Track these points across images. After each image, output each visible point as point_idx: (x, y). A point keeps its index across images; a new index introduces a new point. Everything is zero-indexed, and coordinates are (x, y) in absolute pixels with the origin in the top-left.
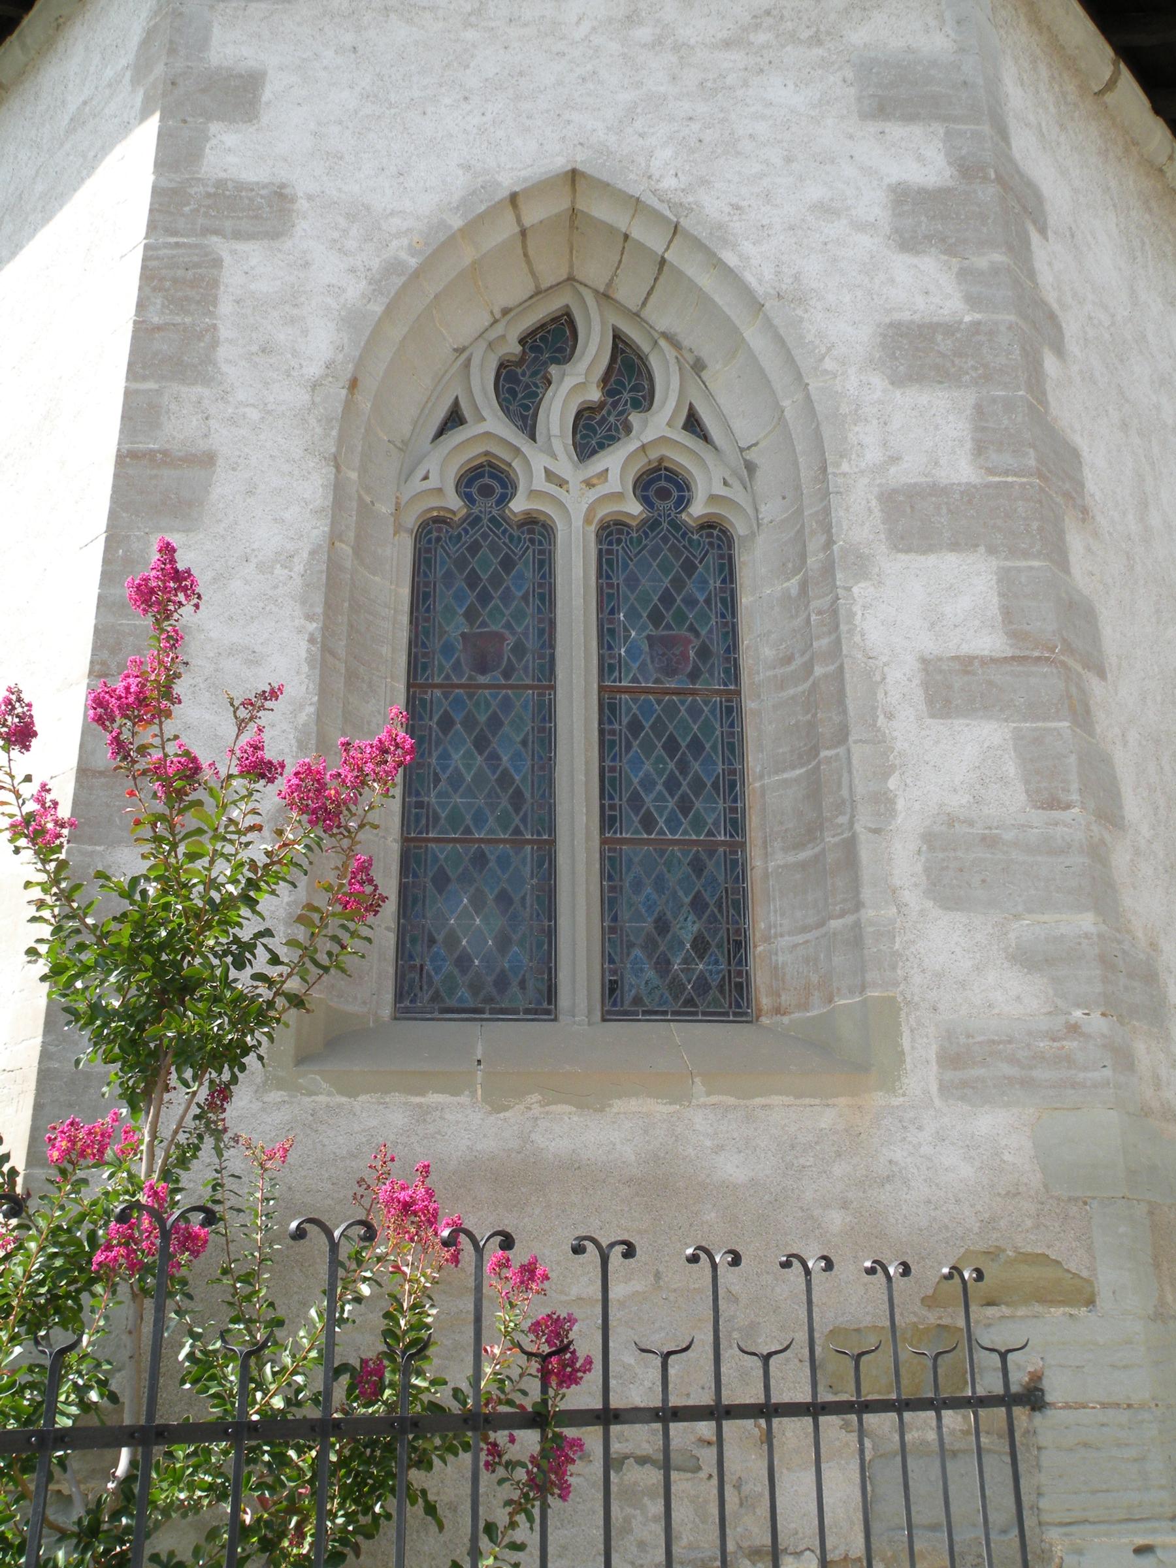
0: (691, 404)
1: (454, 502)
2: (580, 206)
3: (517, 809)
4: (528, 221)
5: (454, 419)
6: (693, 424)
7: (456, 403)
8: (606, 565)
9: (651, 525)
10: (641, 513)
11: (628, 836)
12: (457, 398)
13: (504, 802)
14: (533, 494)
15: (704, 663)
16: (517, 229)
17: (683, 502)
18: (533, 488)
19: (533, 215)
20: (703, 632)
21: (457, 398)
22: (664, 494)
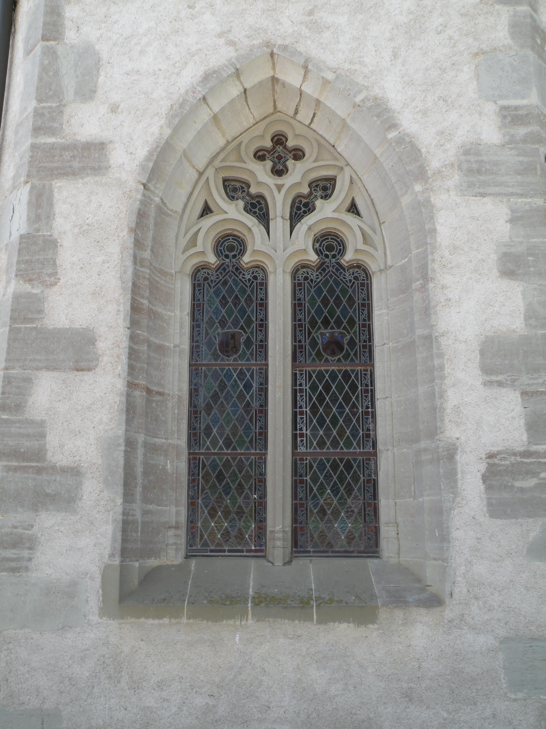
0: (353, 199)
1: (212, 259)
2: (279, 76)
3: (247, 412)
4: (248, 86)
5: (206, 210)
6: (353, 209)
7: (206, 203)
8: (297, 287)
9: (221, 268)
10: (216, 261)
11: (203, 451)
12: (206, 200)
13: (241, 410)
14: (356, 251)
15: (248, 350)
16: (243, 90)
17: (342, 251)
18: (255, 249)
19: (250, 81)
20: (248, 331)
21: (206, 200)
22: (330, 248)
